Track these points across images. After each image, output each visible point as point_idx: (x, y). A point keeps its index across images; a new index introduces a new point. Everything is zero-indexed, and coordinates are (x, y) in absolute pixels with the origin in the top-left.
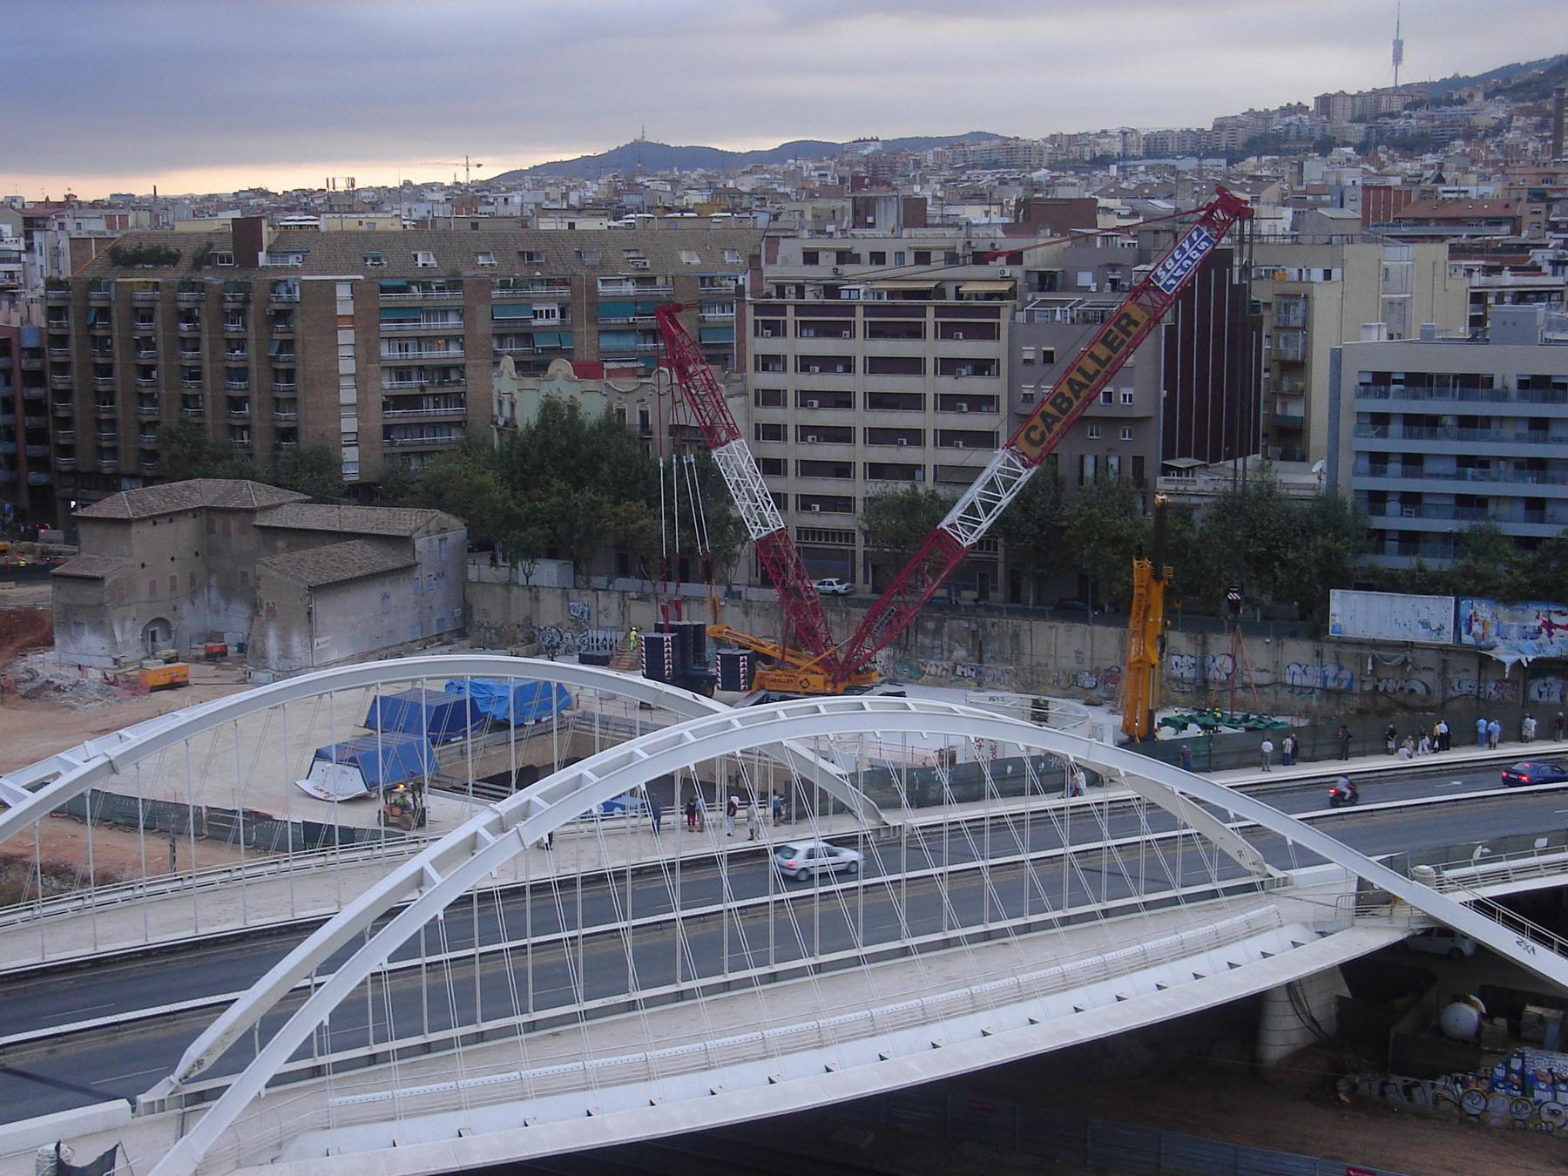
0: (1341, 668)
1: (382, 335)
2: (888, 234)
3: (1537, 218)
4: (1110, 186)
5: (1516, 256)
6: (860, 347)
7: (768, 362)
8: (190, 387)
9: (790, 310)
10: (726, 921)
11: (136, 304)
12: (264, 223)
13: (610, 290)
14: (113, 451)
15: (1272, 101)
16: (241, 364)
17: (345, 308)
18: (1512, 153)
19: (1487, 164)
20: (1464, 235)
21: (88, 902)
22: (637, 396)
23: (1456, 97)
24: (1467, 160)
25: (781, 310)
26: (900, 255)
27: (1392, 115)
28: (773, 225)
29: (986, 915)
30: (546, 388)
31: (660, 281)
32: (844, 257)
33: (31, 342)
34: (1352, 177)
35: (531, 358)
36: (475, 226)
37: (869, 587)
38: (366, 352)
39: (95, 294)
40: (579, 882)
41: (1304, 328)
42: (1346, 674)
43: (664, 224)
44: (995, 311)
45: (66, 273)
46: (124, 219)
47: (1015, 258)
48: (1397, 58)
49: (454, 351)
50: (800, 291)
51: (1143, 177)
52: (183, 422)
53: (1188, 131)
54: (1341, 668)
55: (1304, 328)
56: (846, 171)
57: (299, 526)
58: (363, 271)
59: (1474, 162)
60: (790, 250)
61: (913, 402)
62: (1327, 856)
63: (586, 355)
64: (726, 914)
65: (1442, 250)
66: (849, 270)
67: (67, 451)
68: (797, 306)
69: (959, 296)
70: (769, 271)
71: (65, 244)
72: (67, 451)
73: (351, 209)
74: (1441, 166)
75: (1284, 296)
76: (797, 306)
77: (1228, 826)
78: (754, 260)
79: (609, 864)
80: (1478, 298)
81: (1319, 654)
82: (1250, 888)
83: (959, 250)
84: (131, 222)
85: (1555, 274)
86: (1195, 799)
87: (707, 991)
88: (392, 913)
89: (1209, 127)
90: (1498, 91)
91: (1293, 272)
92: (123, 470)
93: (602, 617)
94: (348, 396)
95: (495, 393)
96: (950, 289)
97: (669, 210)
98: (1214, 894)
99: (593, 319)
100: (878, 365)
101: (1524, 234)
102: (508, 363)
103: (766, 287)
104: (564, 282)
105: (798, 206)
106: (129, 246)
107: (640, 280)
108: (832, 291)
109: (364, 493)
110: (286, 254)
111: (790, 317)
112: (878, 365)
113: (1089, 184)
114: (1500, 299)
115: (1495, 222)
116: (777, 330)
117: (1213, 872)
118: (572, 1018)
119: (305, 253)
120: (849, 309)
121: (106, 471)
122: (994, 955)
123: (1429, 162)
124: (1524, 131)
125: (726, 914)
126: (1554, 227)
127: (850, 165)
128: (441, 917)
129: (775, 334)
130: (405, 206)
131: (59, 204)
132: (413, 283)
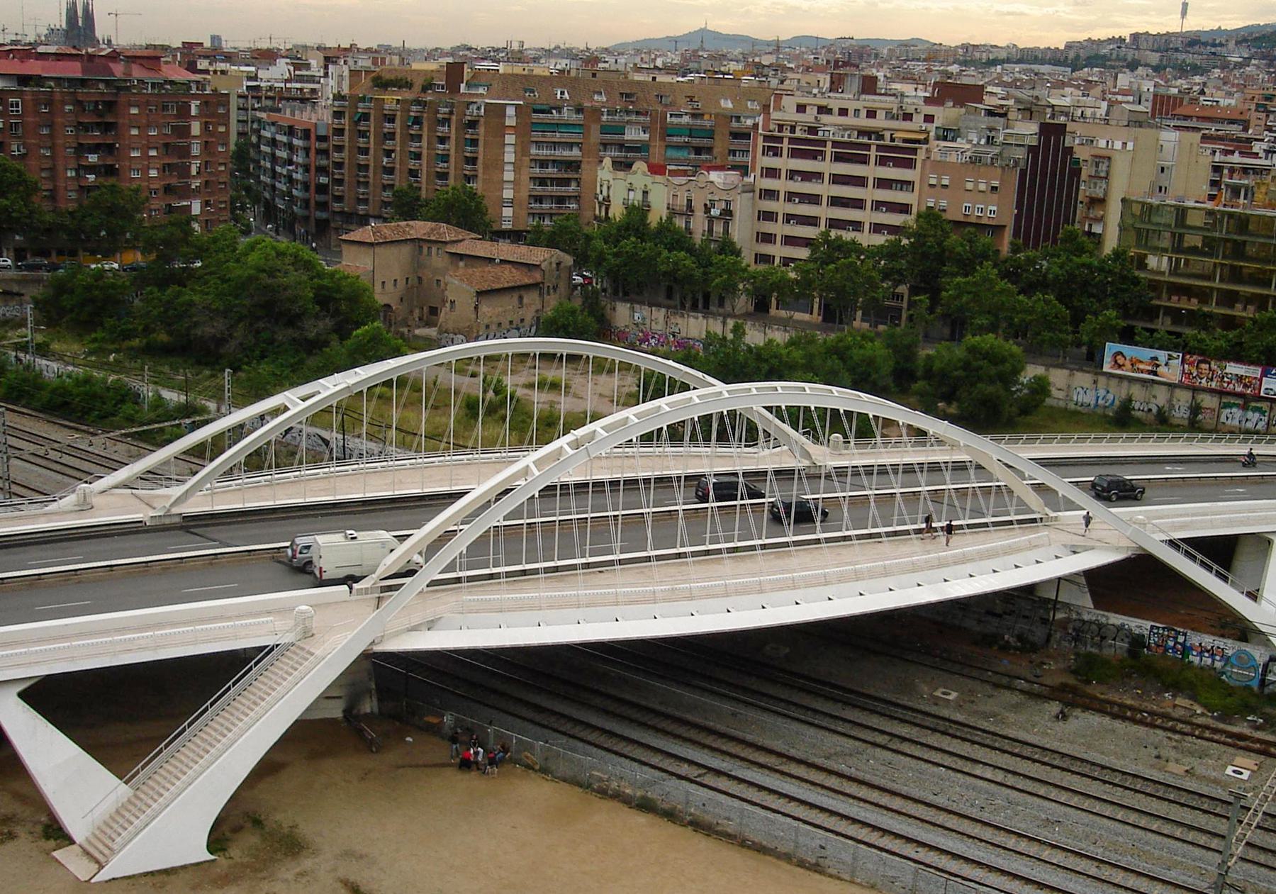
0: (1108, 392)
1: (533, 139)
2: (851, 96)
3: (1259, 122)
4: (994, 79)
5: (1244, 146)
6: (828, 167)
7: (772, 173)
8: (412, 164)
9: (786, 141)
10: (709, 513)
11: (385, 112)
12: (465, 66)
13: (675, 120)
14: (366, 201)
15: (1101, 34)
16: (445, 152)
17: (511, 121)
18: (1250, 78)
19: (1233, 85)
20: (1213, 129)
21: (332, 469)
22: (686, 187)
23: (1217, 42)
24: (1221, 82)
25: (780, 140)
26: (857, 111)
27: (1177, 50)
28: (781, 87)
29: (870, 523)
30: (631, 178)
31: (706, 117)
32: (823, 110)
33: (322, 132)
34: (1148, 86)
35: (623, 160)
36: (594, 75)
37: (820, 318)
38: (522, 149)
39: (361, 105)
40: (653, 481)
41: (1106, 178)
42: (1110, 397)
43: (712, 81)
44: (914, 151)
45: (346, 91)
46: (383, 60)
47: (929, 118)
48: (1184, 13)
49: (576, 152)
50: (793, 129)
51: (1017, 75)
52: (410, 186)
53: (1049, 48)
54: (1108, 392)
55: (1106, 178)
56: (830, 57)
57: (473, 254)
58: (523, 98)
59: (1225, 83)
60: (789, 103)
61: (858, 204)
62: (1078, 503)
63: (656, 160)
64: (710, 510)
65: (1197, 137)
66: (825, 118)
67: (339, 199)
68: (790, 138)
69: (892, 140)
70: (775, 115)
71: (346, 73)
72: (339, 199)
73: (520, 60)
74: (1205, 84)
75: (1096, 156)
76: (790, 138)
77: (1025, 482)
78: (766, 108)
79: (642, 474)
80: (1217, 169)
81: (1095, 382)
82: (1034, 521)
83: (895, 111)
84: (387, 62)
85: (1266, 158)
86: (1006, 465)
87: (694, 554)
88: (507, 491)
89: (1062, 47)
90: (1245, 40)
91: (1102, 144)
92: (371, 213)
93: (653, 323)
94: (509, 176)
95: (599, 179)
96: (887, 135)
97: (716, 73)
98: (1011, 523)
99: (662, 139)
100: (838, 179)
101: (1250, 132)
102: (607, 162)
103: (772, 127)
104: (646, 114)
105: (798, 76)
106: (387, 76)
107: (694, 116)
108: (813, 130)
109: (515, 236)
110: (477, 86)
111: (785, 145)
112: (838, 179)
113: (984, 77)
114: (1232, 170)
115: (1232, 122)
116: (777, 153)
117: (1012, 509)
118: (611, 563)
119: (489, 86)
120: (823, 143)
121: (361, 213)
122: (871, 548)
123: (1197, 81)
124: (1258, 67)
125: (710, 510)
126: (1270, 129)
127: (835, 53)
128: (537, 496)
129: (775, 155)
130: (553, 61)
131: (345, 49)
132: (554, 108)
